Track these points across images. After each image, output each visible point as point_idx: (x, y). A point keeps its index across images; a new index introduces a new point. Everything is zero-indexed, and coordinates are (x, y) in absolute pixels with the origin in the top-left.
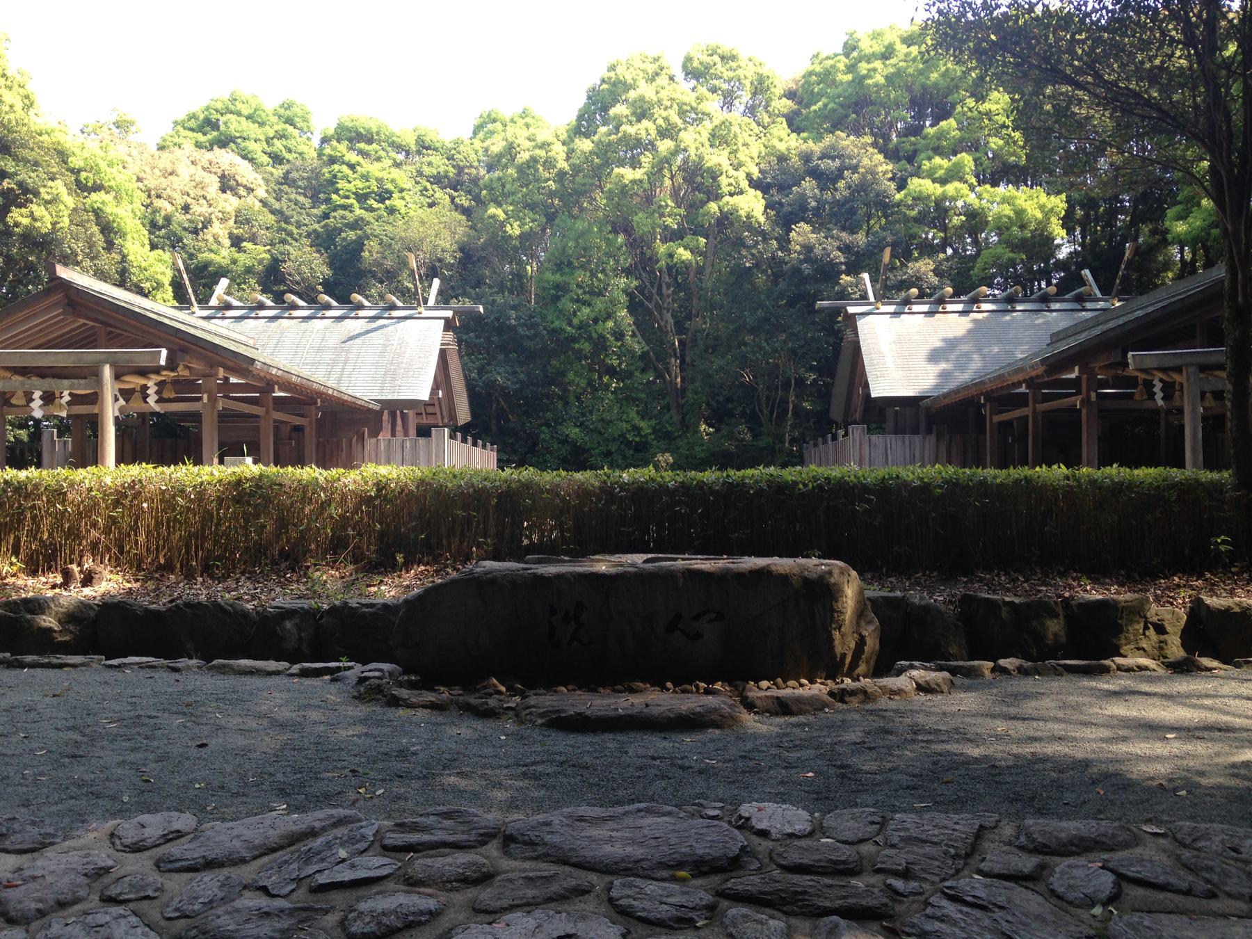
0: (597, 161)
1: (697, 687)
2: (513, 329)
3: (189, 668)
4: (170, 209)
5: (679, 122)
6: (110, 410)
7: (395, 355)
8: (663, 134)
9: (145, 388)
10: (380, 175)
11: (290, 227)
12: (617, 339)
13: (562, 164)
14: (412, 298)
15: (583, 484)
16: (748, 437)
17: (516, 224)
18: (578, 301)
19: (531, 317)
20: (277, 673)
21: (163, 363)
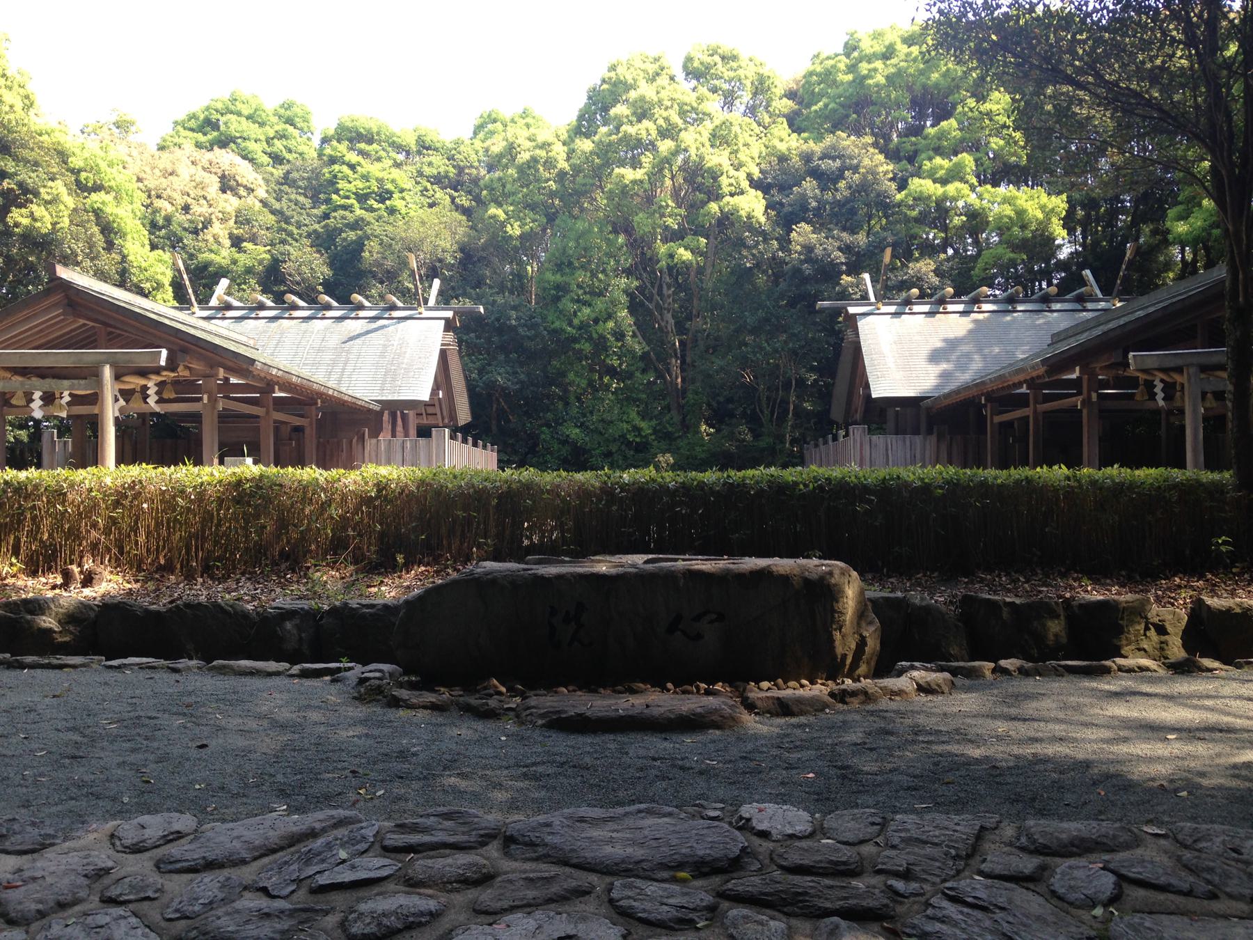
0: (597, 161)
1: (698, 688)
2: (513, 329)
3: (189, 668)
4: (170, 209)
5: (680, 122)
6: (111, 411)
7: (395, 355)
8: (663, 134)
9: (145, 388)
10: (380, 175)
11: (290, 228)
12: (617, 340)
13: (563, 164)
14: (412, 299)
15: (583, 484)
16: (749, 437)
17: (516, 225)
18: (578, 301)
19: (532, 317)
20: (277, 674)
21: (163, 363)
